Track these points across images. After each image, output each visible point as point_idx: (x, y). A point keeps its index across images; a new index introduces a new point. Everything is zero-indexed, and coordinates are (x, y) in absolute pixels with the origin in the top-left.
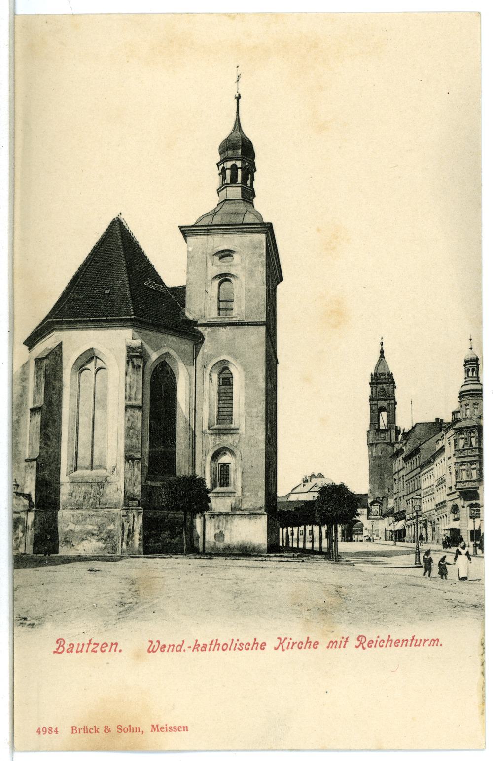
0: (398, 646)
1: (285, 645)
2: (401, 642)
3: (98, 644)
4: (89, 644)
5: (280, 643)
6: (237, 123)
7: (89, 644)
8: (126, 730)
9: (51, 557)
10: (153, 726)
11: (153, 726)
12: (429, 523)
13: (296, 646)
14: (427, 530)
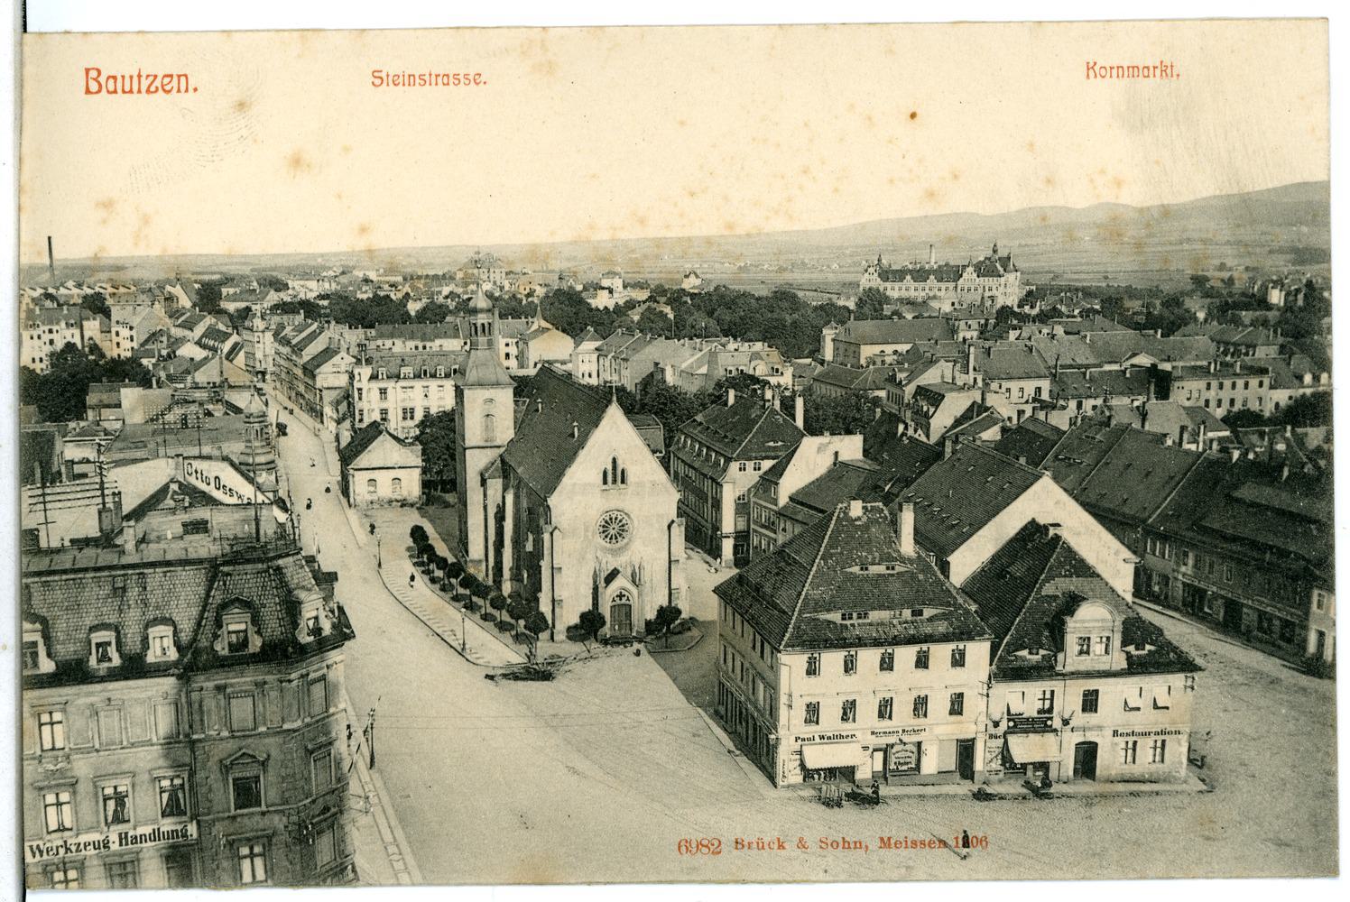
3: (156, 77)
8: (835, 845)
10: (882, 839)
11: (882, 839)
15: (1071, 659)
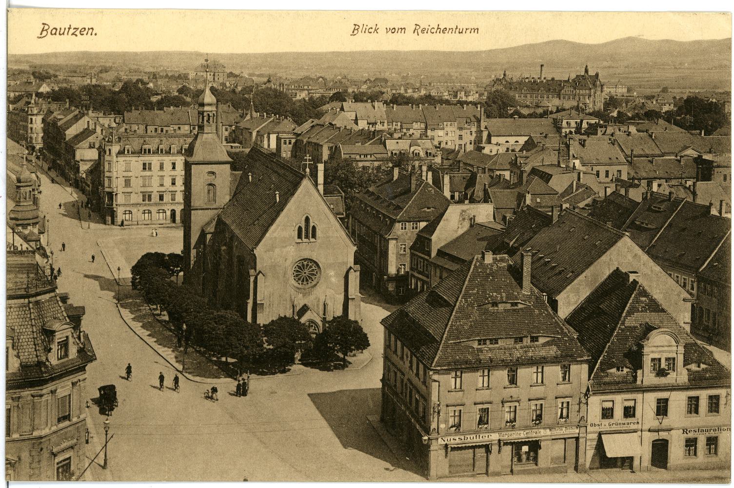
4: (69, 29)
7: (69, 29)
9: (477, 379)
12: (682, 285)
14: (22, 186)
15: (647, 376)
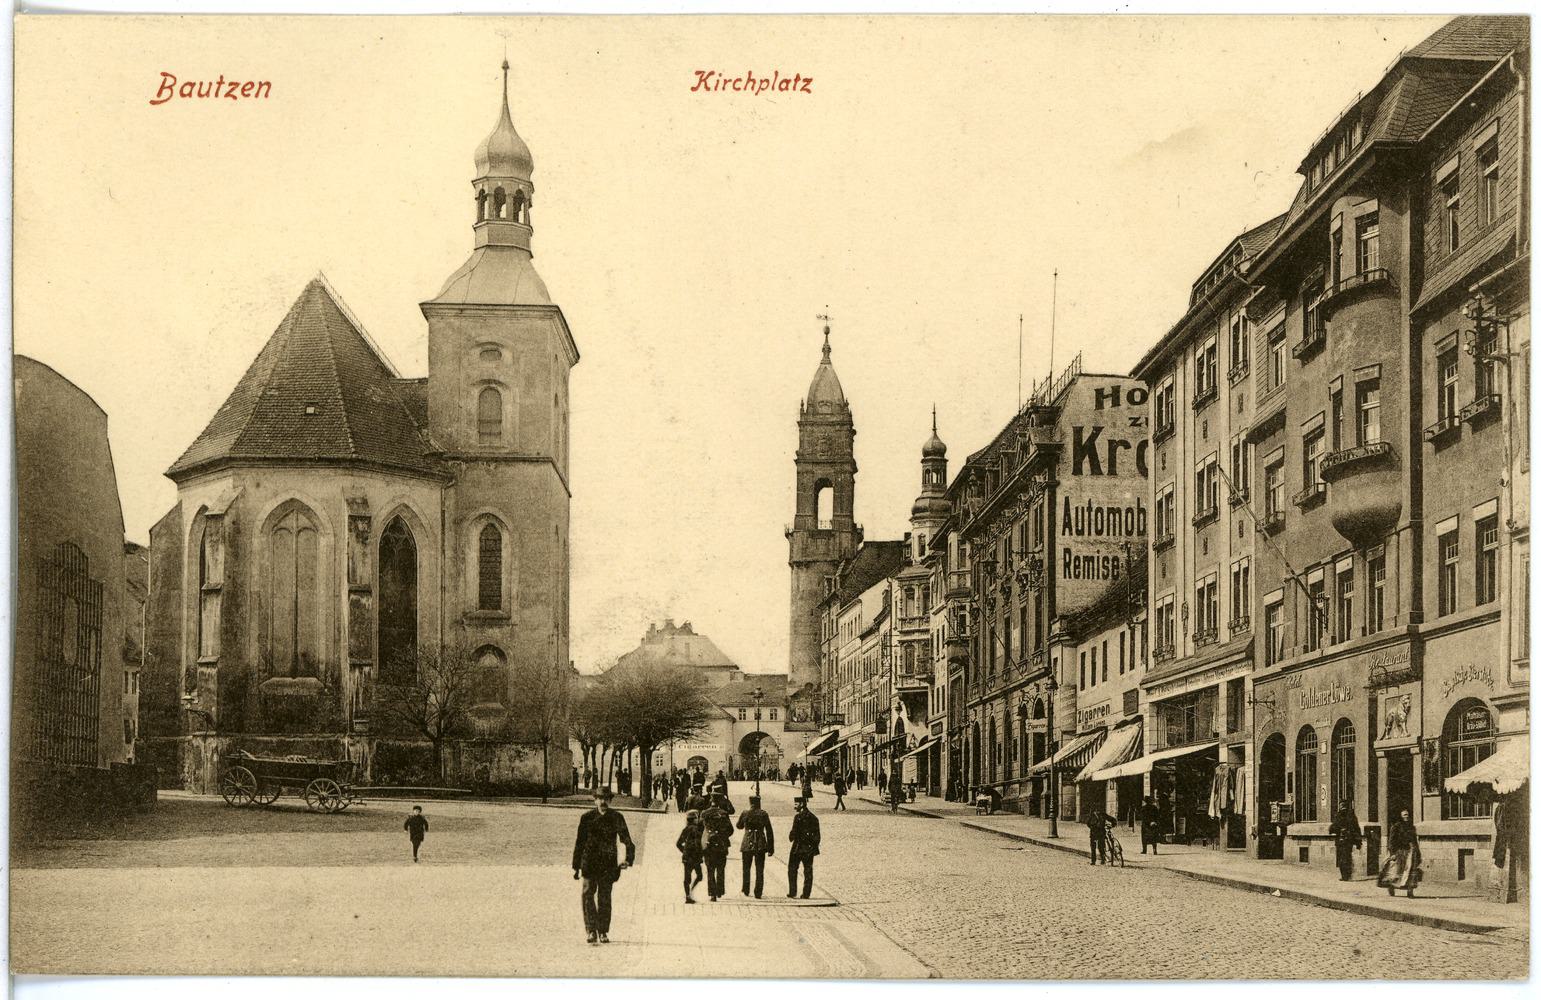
0: (248, 95)
1: (711, 82)
2: (257, 87)
3: (237, 84)
4: (220, 83)
5: (701, 81)
6: (561, 470)
7: (220, 83)
13: (729, 85)
